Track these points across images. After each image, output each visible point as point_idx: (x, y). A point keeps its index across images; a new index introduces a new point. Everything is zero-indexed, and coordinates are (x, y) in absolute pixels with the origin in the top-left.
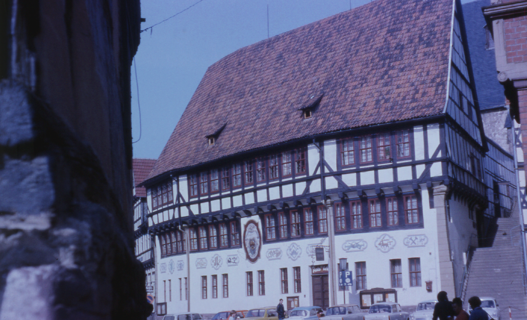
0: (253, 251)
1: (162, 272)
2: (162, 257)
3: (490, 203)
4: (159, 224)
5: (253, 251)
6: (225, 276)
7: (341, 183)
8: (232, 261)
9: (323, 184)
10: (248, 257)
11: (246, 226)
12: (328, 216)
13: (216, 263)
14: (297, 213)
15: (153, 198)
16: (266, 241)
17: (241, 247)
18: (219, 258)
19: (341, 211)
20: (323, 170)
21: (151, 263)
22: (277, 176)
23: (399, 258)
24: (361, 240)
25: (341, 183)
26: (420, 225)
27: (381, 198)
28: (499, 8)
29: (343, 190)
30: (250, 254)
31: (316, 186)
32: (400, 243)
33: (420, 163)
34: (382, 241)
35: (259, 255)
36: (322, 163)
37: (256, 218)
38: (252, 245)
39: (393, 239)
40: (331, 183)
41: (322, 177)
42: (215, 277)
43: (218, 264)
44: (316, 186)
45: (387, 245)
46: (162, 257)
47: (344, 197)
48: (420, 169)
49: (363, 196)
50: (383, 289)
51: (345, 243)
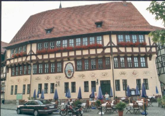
2: (12, 76)
5: (69, 75)
6: (16, 86)
7: (37, 58)
8: (106, 75)
9: (31, 58)
10: (66, 76)
11: (66, 65)
12: (32, 68)
13: (48, 78)
14: (42, 65)
16: (77, 70)
17: (63, 72)
19: (116, 59)
20: (31, 53)
21: (5, 79)
23: (119, 79)
25: (37, 58)
26: (147, 66)
27: (90, 59)
29: (38, 60)
30: (68, 76)
31: (108, 51)
32: (141, 73)
33: (148, 47)
34: (134, 72)
36: (31, 51)
37: (73, 62)
40: (34, 58)
41: (111, 47)
42: (46, 85)
43: (48, 79)
44: (108, 51)
45: (135, 74)
46: (12, 76)
47: (37, 63)
48: (148, 49)
49: (43, 62)
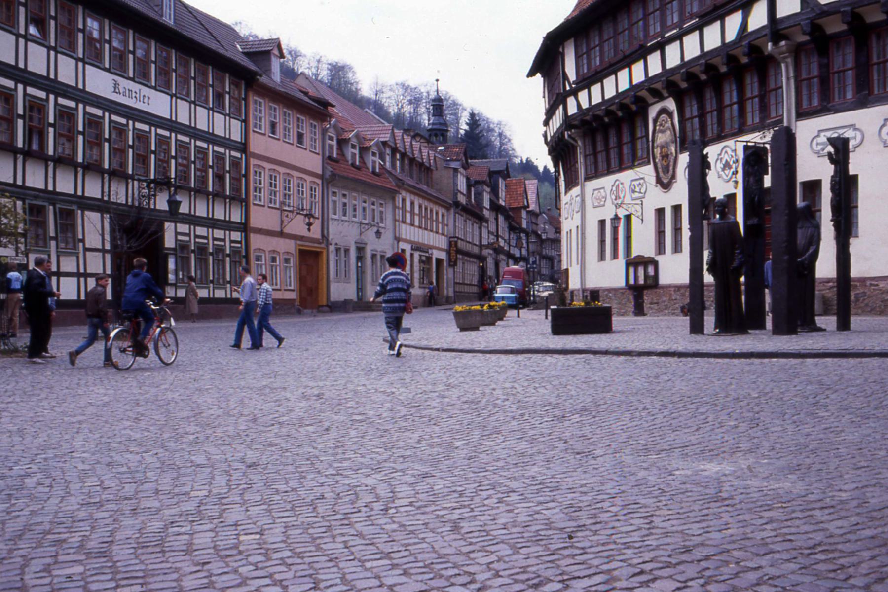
0: (666, 169)
1: (595, 207)
3: (488, 207)
4: (591, 108)
8: (637, 189)
10: (659, 181)
11: (655, 121)
15: (578, 57)
17: (649, 163)
18: (621, 186)
22: (675, 21)
24: (853, 126)
28: (307, 244)
30: (661, 174)
35: (674, 176)
37: (671, 104)
38: (665, 156)
39: (855, 129)
50: (643, 257)
51: (818, 136)
